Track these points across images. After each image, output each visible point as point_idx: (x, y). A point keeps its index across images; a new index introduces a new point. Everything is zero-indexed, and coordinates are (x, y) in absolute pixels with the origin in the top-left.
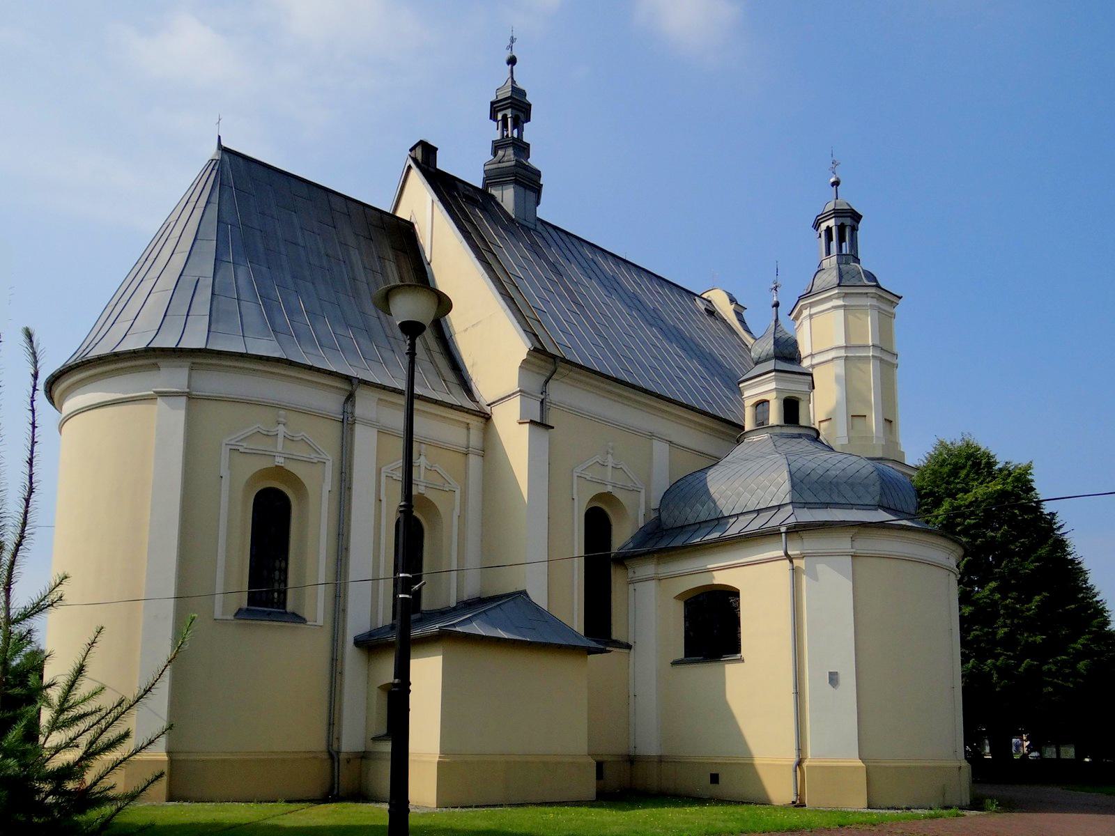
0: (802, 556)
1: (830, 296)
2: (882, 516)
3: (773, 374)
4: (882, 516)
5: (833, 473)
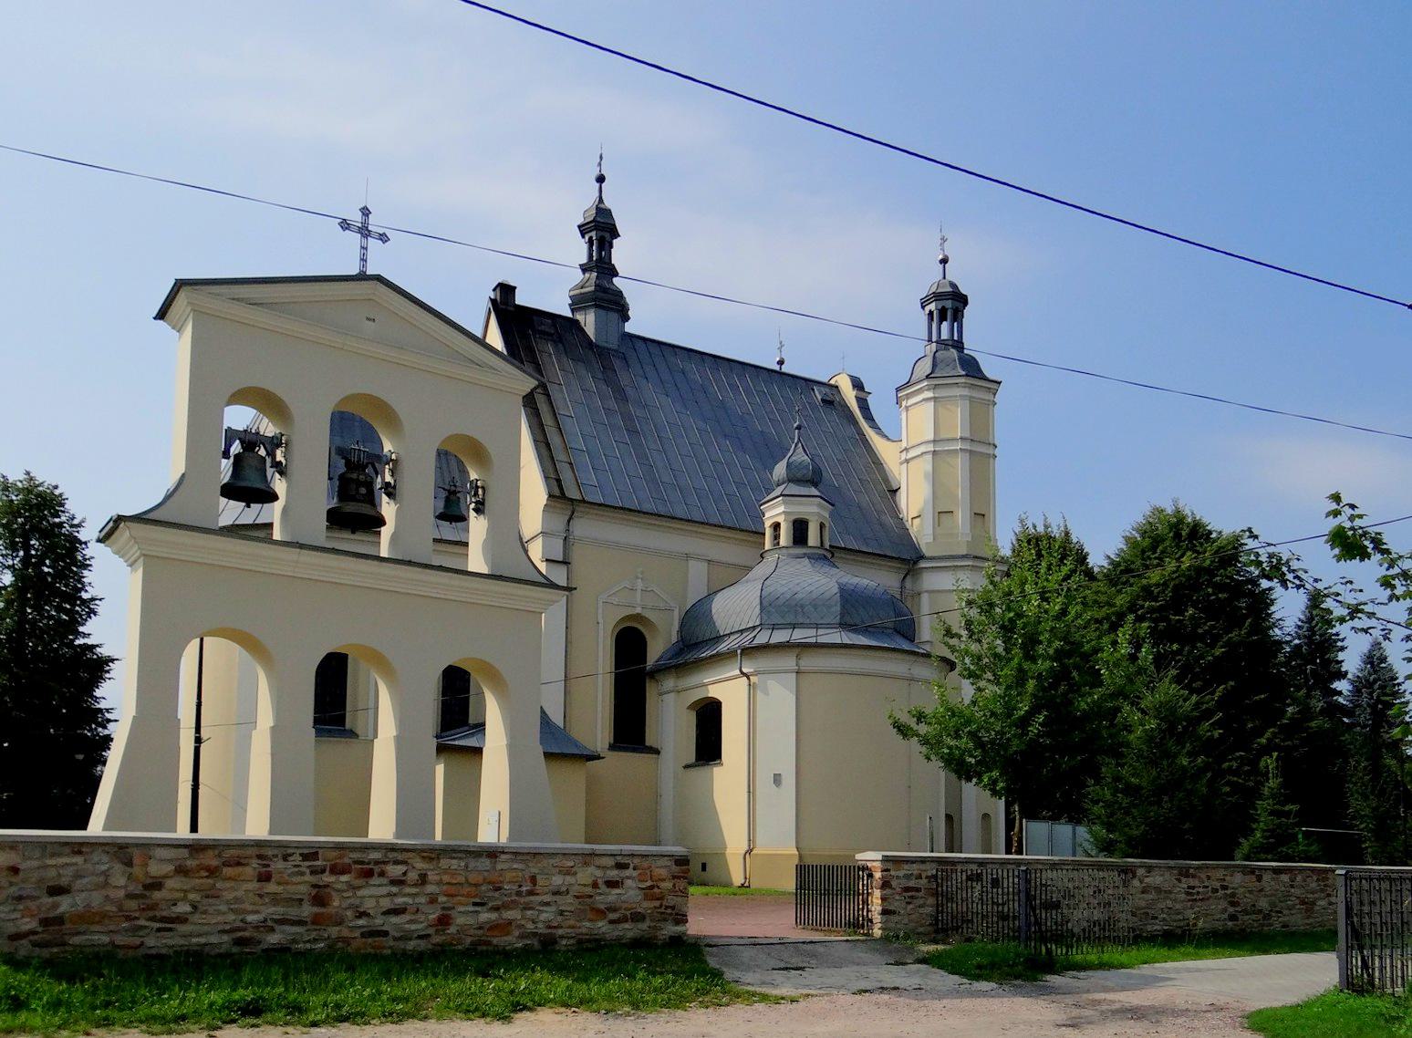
0: (756, 673)
1: (921, 388)
2: (836, 637)
3: (781, 498)
4: (836, 637)
5: (799, 596)
